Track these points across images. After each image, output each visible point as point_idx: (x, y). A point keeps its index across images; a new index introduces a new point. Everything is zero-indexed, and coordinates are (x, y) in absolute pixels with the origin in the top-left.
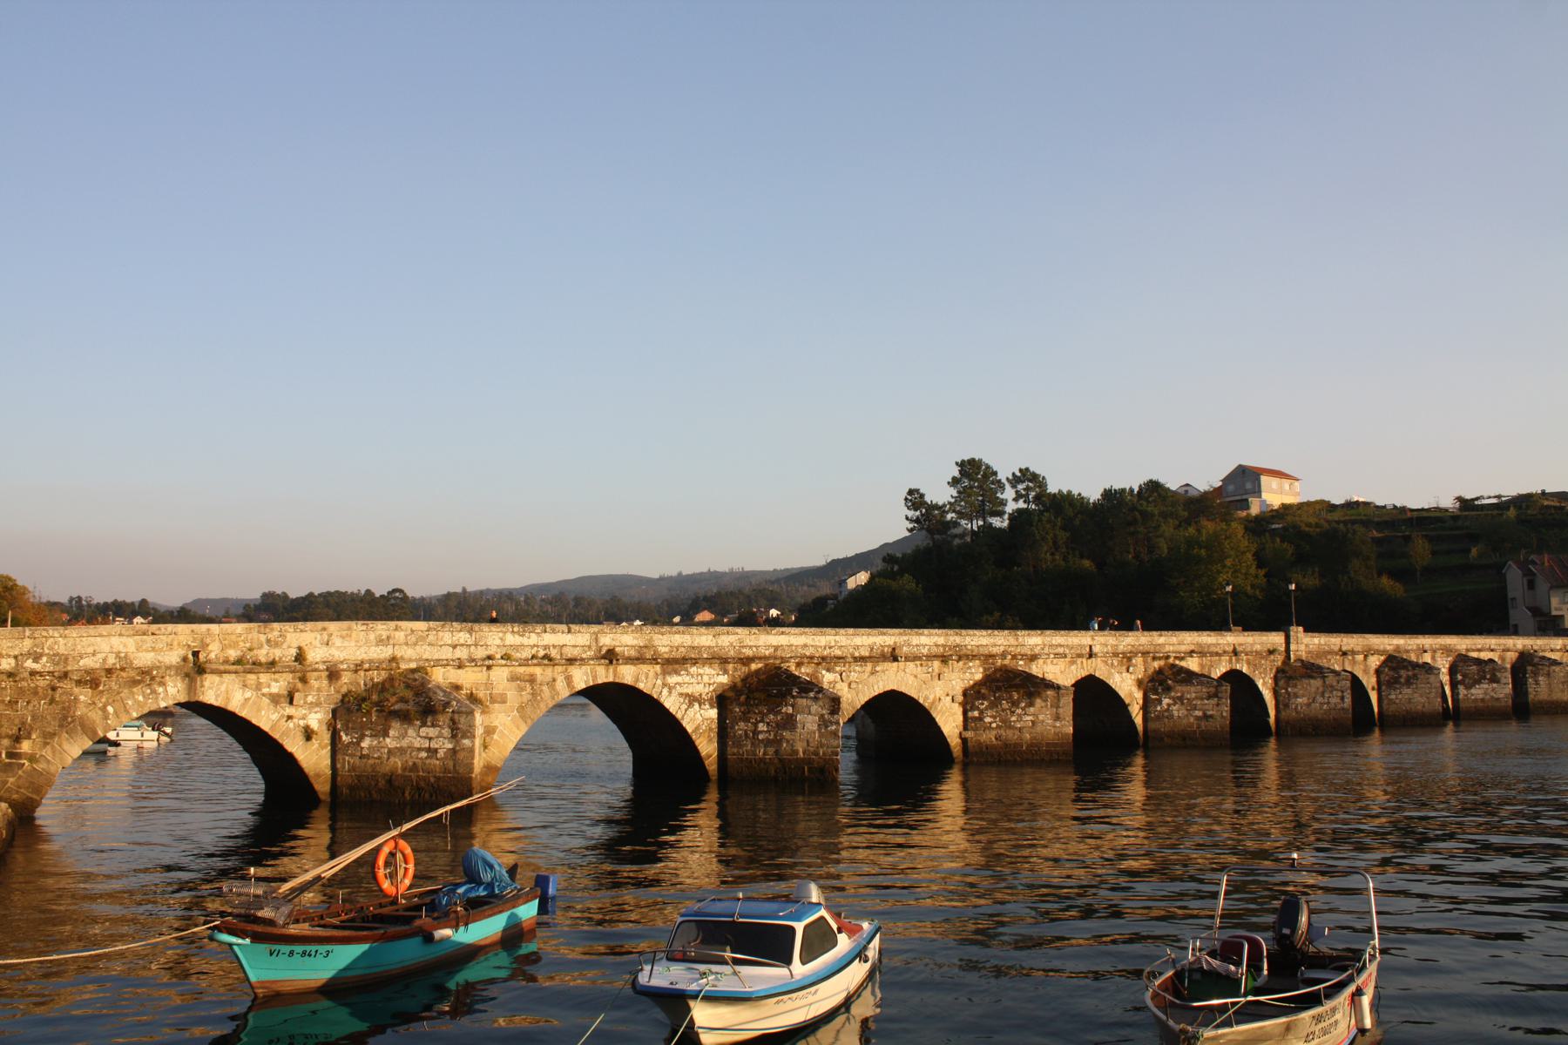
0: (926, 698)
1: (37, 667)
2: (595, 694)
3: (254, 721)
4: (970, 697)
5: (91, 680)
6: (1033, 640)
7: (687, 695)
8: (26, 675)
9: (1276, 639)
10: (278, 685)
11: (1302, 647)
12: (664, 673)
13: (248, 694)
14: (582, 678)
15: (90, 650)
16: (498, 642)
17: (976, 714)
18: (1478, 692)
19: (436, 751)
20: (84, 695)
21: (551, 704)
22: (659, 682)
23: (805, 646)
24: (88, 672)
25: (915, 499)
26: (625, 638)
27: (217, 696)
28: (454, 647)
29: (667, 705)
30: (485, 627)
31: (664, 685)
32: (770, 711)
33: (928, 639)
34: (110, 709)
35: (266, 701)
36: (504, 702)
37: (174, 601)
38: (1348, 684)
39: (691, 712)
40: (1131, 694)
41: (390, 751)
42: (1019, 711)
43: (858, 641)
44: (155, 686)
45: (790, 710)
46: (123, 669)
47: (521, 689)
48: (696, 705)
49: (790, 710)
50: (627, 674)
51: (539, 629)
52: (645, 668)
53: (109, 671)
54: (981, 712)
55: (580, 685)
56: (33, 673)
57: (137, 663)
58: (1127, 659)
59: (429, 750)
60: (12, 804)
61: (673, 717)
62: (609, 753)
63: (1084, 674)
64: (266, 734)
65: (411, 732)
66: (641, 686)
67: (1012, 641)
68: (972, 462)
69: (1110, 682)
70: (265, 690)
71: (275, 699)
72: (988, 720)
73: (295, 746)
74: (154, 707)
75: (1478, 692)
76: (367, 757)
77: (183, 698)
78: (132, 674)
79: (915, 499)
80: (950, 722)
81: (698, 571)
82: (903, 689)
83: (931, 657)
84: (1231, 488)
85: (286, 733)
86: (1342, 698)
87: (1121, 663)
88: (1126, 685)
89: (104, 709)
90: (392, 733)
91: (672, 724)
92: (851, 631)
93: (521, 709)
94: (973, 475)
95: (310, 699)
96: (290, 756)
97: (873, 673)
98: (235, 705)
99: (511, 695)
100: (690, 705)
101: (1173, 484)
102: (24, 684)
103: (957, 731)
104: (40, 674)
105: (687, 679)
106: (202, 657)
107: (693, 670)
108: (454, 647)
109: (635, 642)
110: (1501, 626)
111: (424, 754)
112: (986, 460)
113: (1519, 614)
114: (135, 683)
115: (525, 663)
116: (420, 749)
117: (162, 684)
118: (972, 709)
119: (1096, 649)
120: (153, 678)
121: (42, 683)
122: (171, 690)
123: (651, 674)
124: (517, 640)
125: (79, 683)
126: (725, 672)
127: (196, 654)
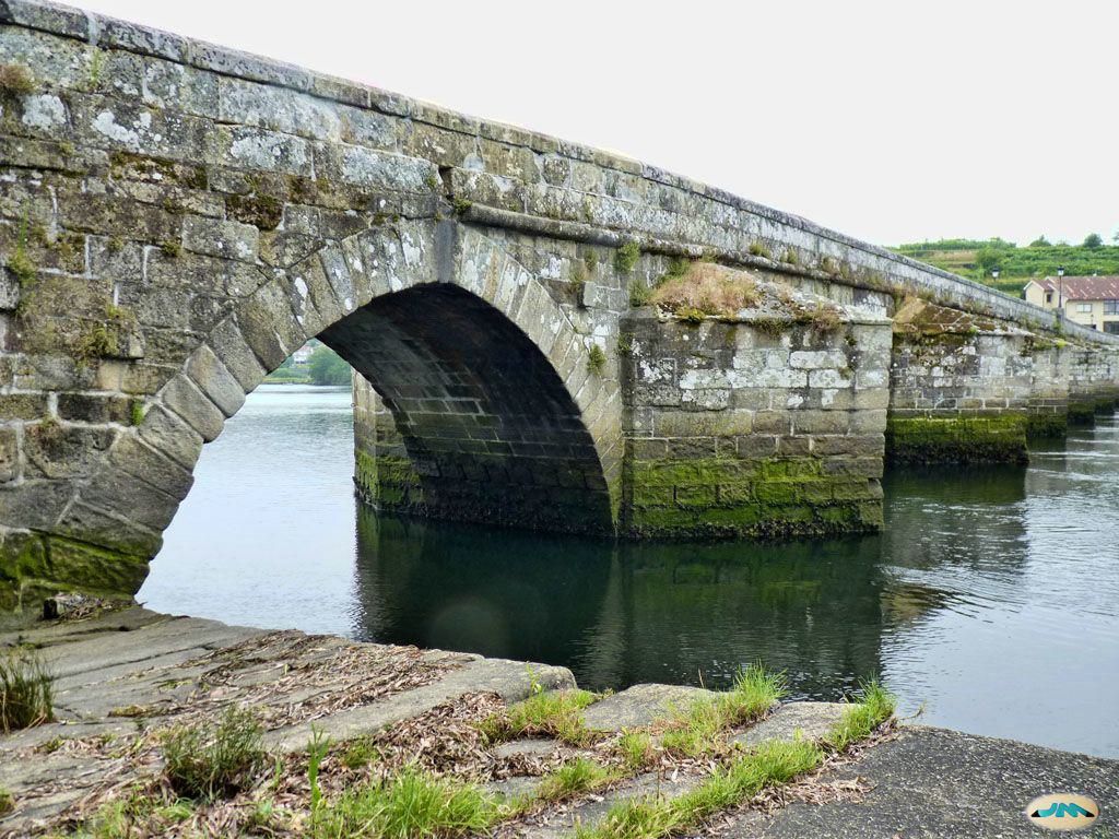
3: (532, 337)
8: (101, 157)
10: (558, 268)
15: (253, 117)
20: (245, 240)
27: (482, 275)
32: (948, 353)
35: (545, 294)
41: (734, 399)
44: (383, 239)
49: (972, 351)
56: (120, 156)
59: (805, 391)
65: (773, 359)
70: (544, 272)
74: (381, 291)
76: (693, 408)
89: (289, 290)
90: (737, 362)
101: (1054, 241)
102: (96, 186)
111: (797, 400)
114: (347, 225)
117: (396, 235)
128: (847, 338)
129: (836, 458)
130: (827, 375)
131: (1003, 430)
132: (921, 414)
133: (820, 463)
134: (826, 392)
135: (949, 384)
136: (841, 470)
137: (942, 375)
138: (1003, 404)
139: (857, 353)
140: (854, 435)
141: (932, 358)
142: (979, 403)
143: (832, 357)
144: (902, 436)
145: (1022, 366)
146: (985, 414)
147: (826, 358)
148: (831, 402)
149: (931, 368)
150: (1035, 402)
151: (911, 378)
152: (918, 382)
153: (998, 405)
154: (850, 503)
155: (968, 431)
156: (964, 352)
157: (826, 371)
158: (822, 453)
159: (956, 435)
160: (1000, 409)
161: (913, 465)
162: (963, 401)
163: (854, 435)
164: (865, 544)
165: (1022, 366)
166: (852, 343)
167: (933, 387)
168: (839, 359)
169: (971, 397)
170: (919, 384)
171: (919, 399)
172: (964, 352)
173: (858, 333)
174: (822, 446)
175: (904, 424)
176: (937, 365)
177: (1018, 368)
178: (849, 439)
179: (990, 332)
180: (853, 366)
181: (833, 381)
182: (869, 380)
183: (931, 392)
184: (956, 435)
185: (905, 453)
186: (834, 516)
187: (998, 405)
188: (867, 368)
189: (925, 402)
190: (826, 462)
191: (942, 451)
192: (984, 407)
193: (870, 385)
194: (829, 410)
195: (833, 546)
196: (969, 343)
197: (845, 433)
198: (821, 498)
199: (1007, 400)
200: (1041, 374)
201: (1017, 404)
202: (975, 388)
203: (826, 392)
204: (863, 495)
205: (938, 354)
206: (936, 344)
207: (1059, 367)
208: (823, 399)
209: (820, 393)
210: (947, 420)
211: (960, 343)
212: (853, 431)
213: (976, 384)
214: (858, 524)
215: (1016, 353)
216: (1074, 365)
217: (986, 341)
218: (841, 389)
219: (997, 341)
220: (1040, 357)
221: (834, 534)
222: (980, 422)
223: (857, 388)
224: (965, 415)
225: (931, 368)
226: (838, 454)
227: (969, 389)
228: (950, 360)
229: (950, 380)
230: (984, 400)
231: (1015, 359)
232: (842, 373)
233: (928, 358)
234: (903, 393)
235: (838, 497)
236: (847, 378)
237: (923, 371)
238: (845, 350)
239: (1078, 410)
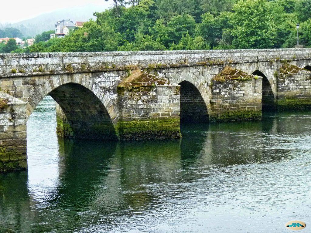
0: (198, 84)
4: (214, 84)
7: (104, 88)
12: (93, 77)
16: (16, 63)
17: (218, 91)
22: (91, 81)
23: (151, 60)
29: (95, 93)
31: (94, 83)
32: (144, 94)
39: (105, 97)
40: (272, 78)
42: (237, 89)
45: (154, 93)
47: (29, 89)
49: (154, 93)
50: (77, 79)
52: (84, 75)
54: (220, 90)
58: (270, 63)
62: (156, 176)
66: (83, 84)
72: (223, 93)
82: (189, 80)
87: (269, 65)
99: (24, 92)
100: (105, 93)
103: (209, 100)
105: (103, 79)
107: (105, 74)
109: (80, 61)
115: (30, 53)
118: (215, 89)
119: (260, 58)
123: (88, 77)
126: (119, 75)
128: (11, 109)
129: (10, 147)
130: (5, 121)
131: (170, 125)
132: (134, 120)
133: (5, 149)
134: (5, 126)
135: (145, 107)
136: (12, 151)
137: (142, 103)
138: (169, 115)
139: (15, 114)
140: (16, 140)
141: (138, 97)
142: (159, 114)
143: (6, 116)
144: (127, 129)
145: (176, 99)
146: (160, 119)
147: (4, 116)
148: (7, 130)
149: (138, 100)
150: (245, 105)
151: (129, 105)
152: (132, 107)
153: (166, 115)
154: (16, 161)
155: (155, 126)
156: (151, 94)
157: (5, 120)
158: (5, 146)
159: (150, 128)
160: (167, 116)
161: (131, 140)
162: (151, 114)
163: (16, 140)
164: (21, 174)
165: (176, 99)
166: (13, 111)
167: (138, 109)
168: (8, 116)
169: (155, 112)
170: (132, 108)
171: (132, 114)
172: (151, 94)
173: (15, 108)
174: (5, 143)
175: (127, 124)
176: (140, 99)
177: (174, 100)
178: (14, 141)
179: (161, 85)
180: (13, 118)
181: (7, 123)
182: (19, 122)
183: (137, 111)
184: (150, 128)
185: (128, 136)
186: (11, 165)
187: (166, 115)
188: (18, 119)
189: (135, 115)
190: (6, 148)
191: (143, 134)
192: (161, 116)
193: (20, 124)
194: (7, 132)
195: (11, 175)
196: (153, 90)
197: (13, 139)
198: (6, 159)
199: (170, 113)
200: (247, 92)
201: (174, 114)
202: (156, 108)
203: (5, 126)
204: (20, 158)
205: (140, 95)
206: (139, 91)
207: (257, 88)
208: (4, 129)
209: (3, 127)
210: (145, 122)
211: (149, 90)
212: (15, 138)
213: (157, 107)
214: (18, 167)
215: (173, 94)
216: (303, 80)
217: (160, 89)
218: (10, 126)
219: (164, 89)
220: (246, 84)
221: (10, 171)
222: (159, 122)
223: (15, 125)
224: (153, 119)
225: (137, 101)
226: (10, 146)
227: (154, 109)
228: (145, 97)
229: (146, 105)
230: (160, 113)
231: (173, 96)
232: (10, 120)
233: (136, 97)
234: (126, 111)
235: (11, 159)
236: (12, 122)
237: (134, 102)
238: (11, 113)
239: (306, 103)
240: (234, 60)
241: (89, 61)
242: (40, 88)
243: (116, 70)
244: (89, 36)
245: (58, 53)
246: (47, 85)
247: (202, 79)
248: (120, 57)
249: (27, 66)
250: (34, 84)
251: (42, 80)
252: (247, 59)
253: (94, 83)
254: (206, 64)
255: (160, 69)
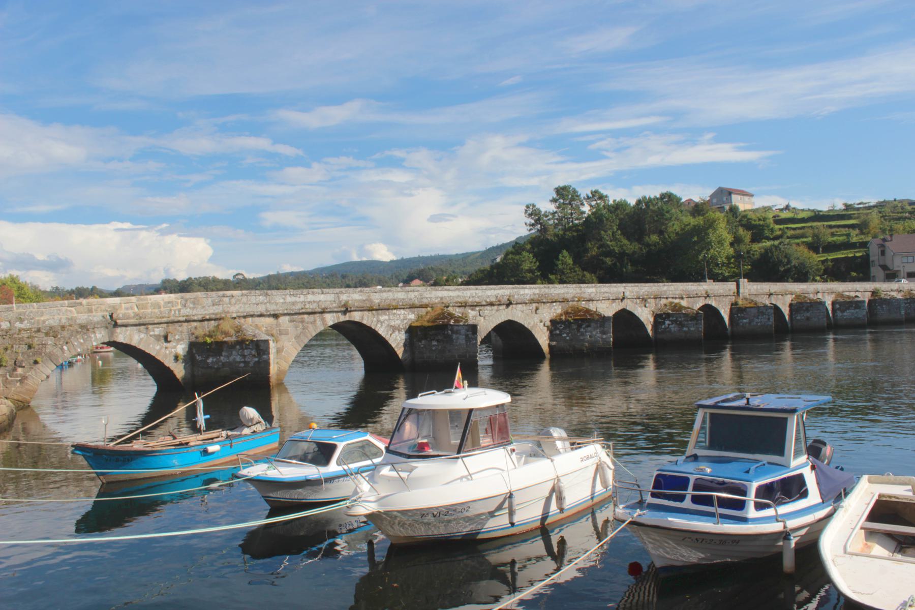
1: (22, 326)
2: (338, 327)
5: (52, 332)
6: (590, 290)
9: (732, 286)
10: (158, 331)
11: (747, 291)
13: (142, 336)
14: (331, 319)
16: (282, 301)
17: (558, 332)
18: (847, 314)
19: (249, 362)
20: (50, 341)
21: (314, 334)
23: (458, 296)
24: (51, 328)
25: (534, 213)
26: (354, 296)
28: (258, 304)
29: (380, 332)
30: (274, 292)
33: (528, 291)
34: (65, 348)
35: (152, 339)
36: (287, 334)
37: (114, 288)
38: (772, 311)
41: (224, 364)
43: (489, 293)
46: (71, 326)
47: (296, 327)
48: (397, 332)
50: (356, 316)
51: (305, 291)
53: (63, 327)
54: (561, 331)
55: (331, 323)
57: (78, 321)
58: (644, 301)
59: (245, 362)
60: (15, 401)
61: (384, 339)
63: (620, 308)
64: (153, 357)
66: (365, 322)
67: (578, 290)
68: (564, 188)
69: (636, 313)
70: (152, 333)
71: (157, 338)
73: (169, 363)
75: (847, 314)
77: (107, 340)
78: (76, 327)
79: (534, 213)
80: (543, 339)
81: (412, 256)
83: (532, 301)
84: (715, 201)
85: (165, 356)
86: (769, 319)
88: (645, 316)
89: (62, 349)
90: (224, 354)
91: (383, 342)
92: (484, 287)
93: (297, 337)
94: (564, 194)
95: (177, 337)
96: (168, 368)
97: (497, 311)
98: (134, 343)
100: (394, 332)
104: (25, 330)
106: (115, 316)
108: (258, 304)
110: (866, 277)
111: (242, 365)
112: (573, 186)
113: (875, 270)
116: (240, 362)
119: (627, 294)
120: (88, 330)
121: (25, 335)
122: (99, 336)
124: (293, 299)
125: (47, 334)
127: (111, 316)
240: (587, 296)
241: (373, 298)
242: (310, 325)
243: (412, 307)
244: (260, 283)
245: (584, 276)
246: (319, 322)
247: (536, 319)
248: (416, 294)
249: (294, 304)
250: (303, 321)
251: (312, 317)
252: (606, 295)
253: (378, 321)
254: (538, 301)
255: (473, 306)
